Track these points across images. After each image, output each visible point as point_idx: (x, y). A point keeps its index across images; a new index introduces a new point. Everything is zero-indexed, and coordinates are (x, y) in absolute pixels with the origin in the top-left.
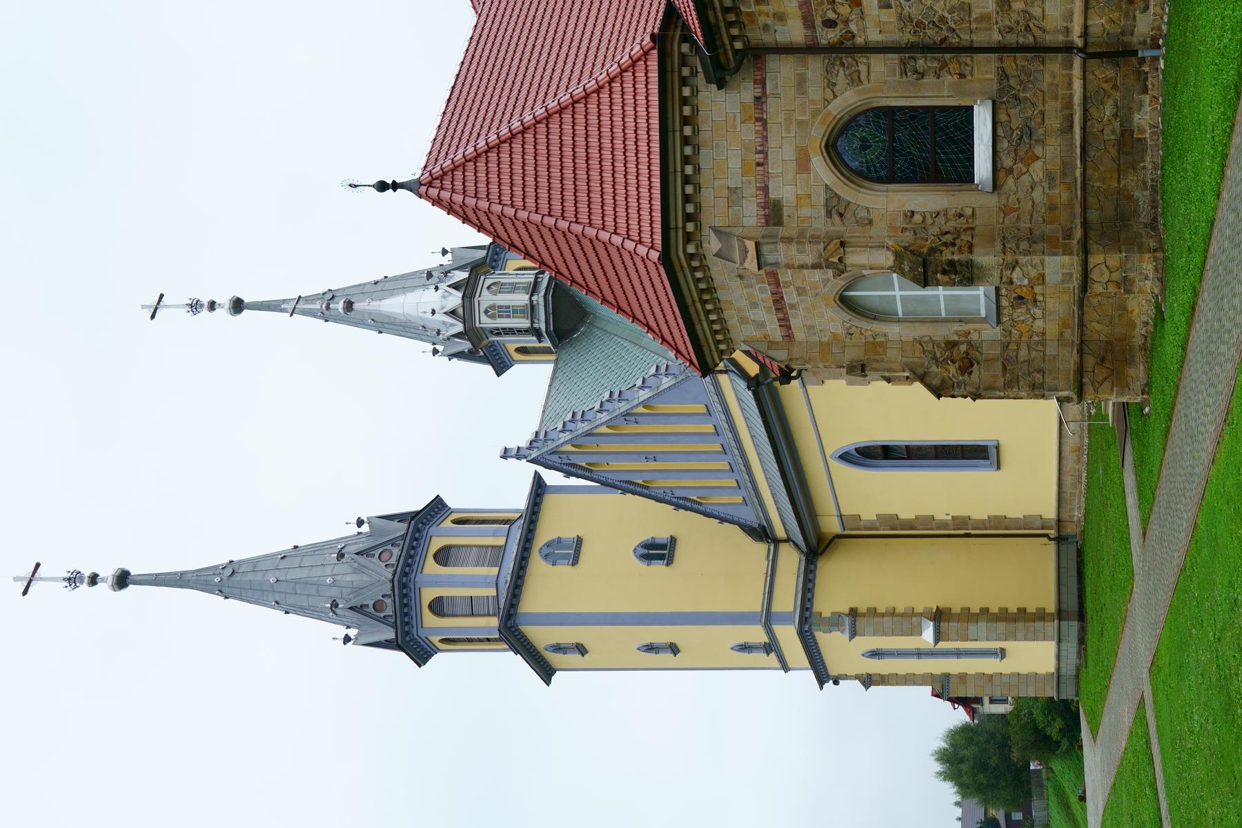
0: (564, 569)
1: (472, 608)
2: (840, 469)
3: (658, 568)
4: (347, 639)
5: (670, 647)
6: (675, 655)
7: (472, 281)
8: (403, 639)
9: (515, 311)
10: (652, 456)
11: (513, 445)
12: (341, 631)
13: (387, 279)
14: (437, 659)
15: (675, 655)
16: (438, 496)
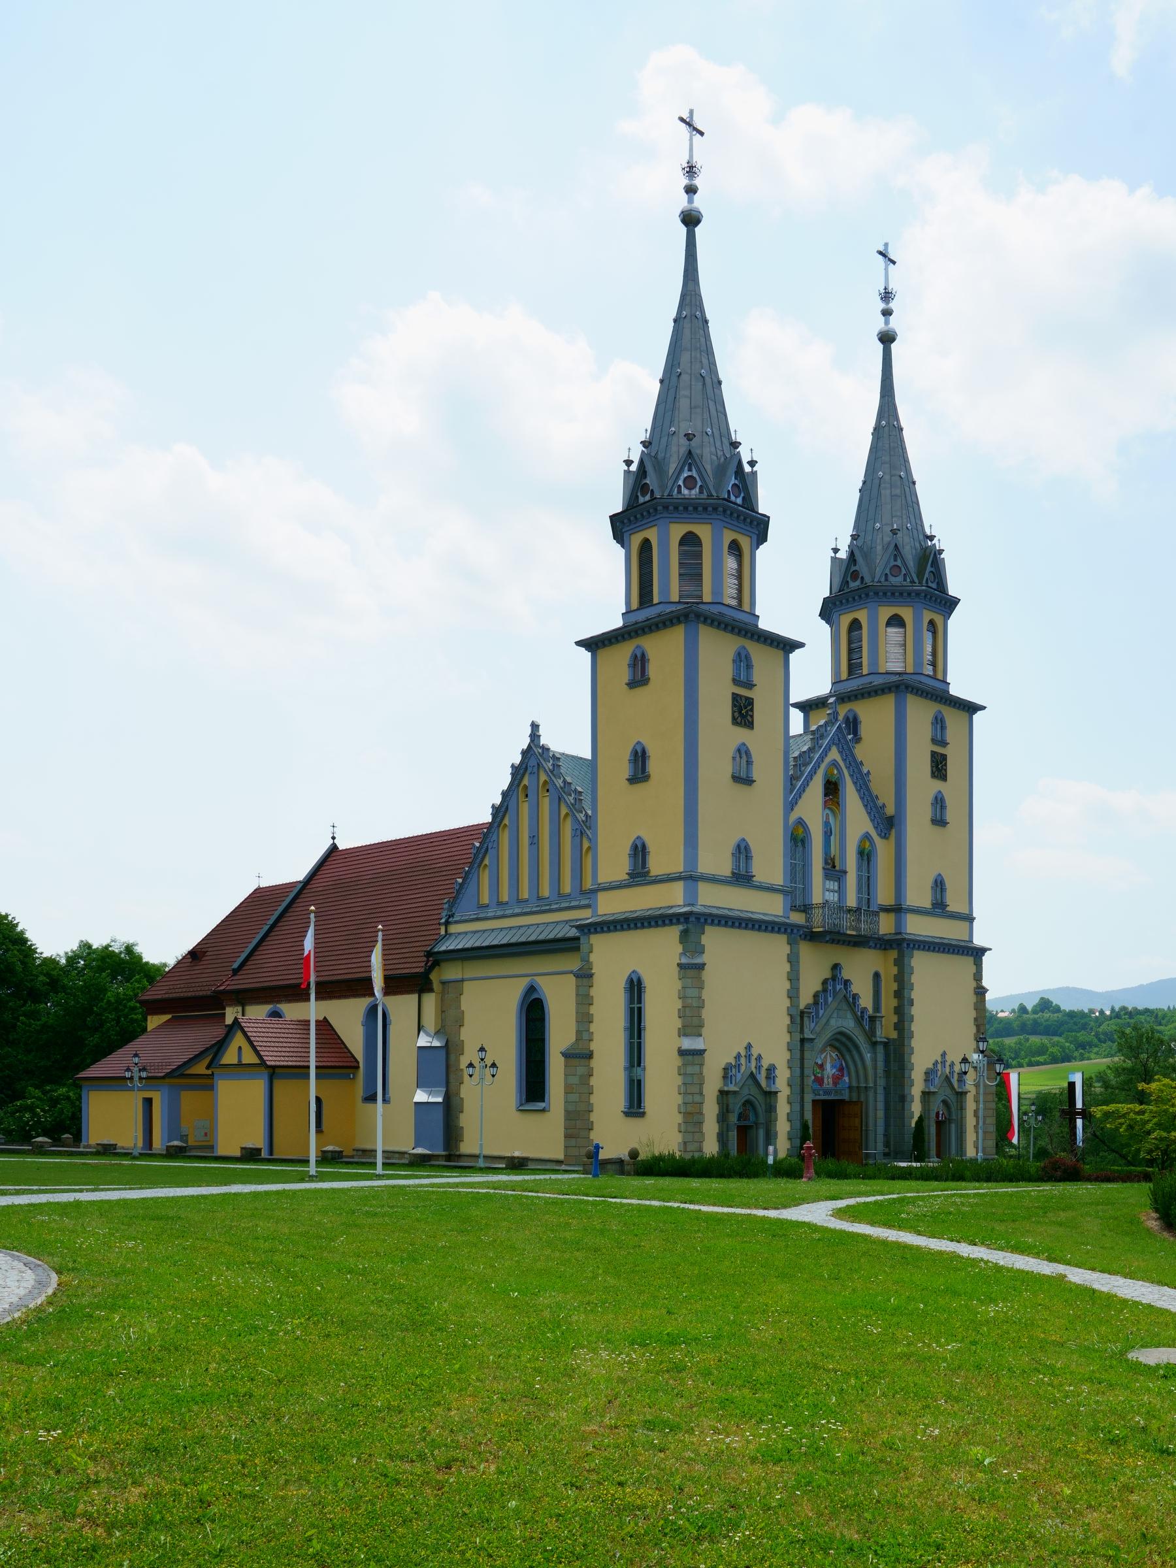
1: (691, 572)
2: (520, 986)
4: (836, 550)
10: (535, 841)
11: (541, 731)
12: (636, 458)
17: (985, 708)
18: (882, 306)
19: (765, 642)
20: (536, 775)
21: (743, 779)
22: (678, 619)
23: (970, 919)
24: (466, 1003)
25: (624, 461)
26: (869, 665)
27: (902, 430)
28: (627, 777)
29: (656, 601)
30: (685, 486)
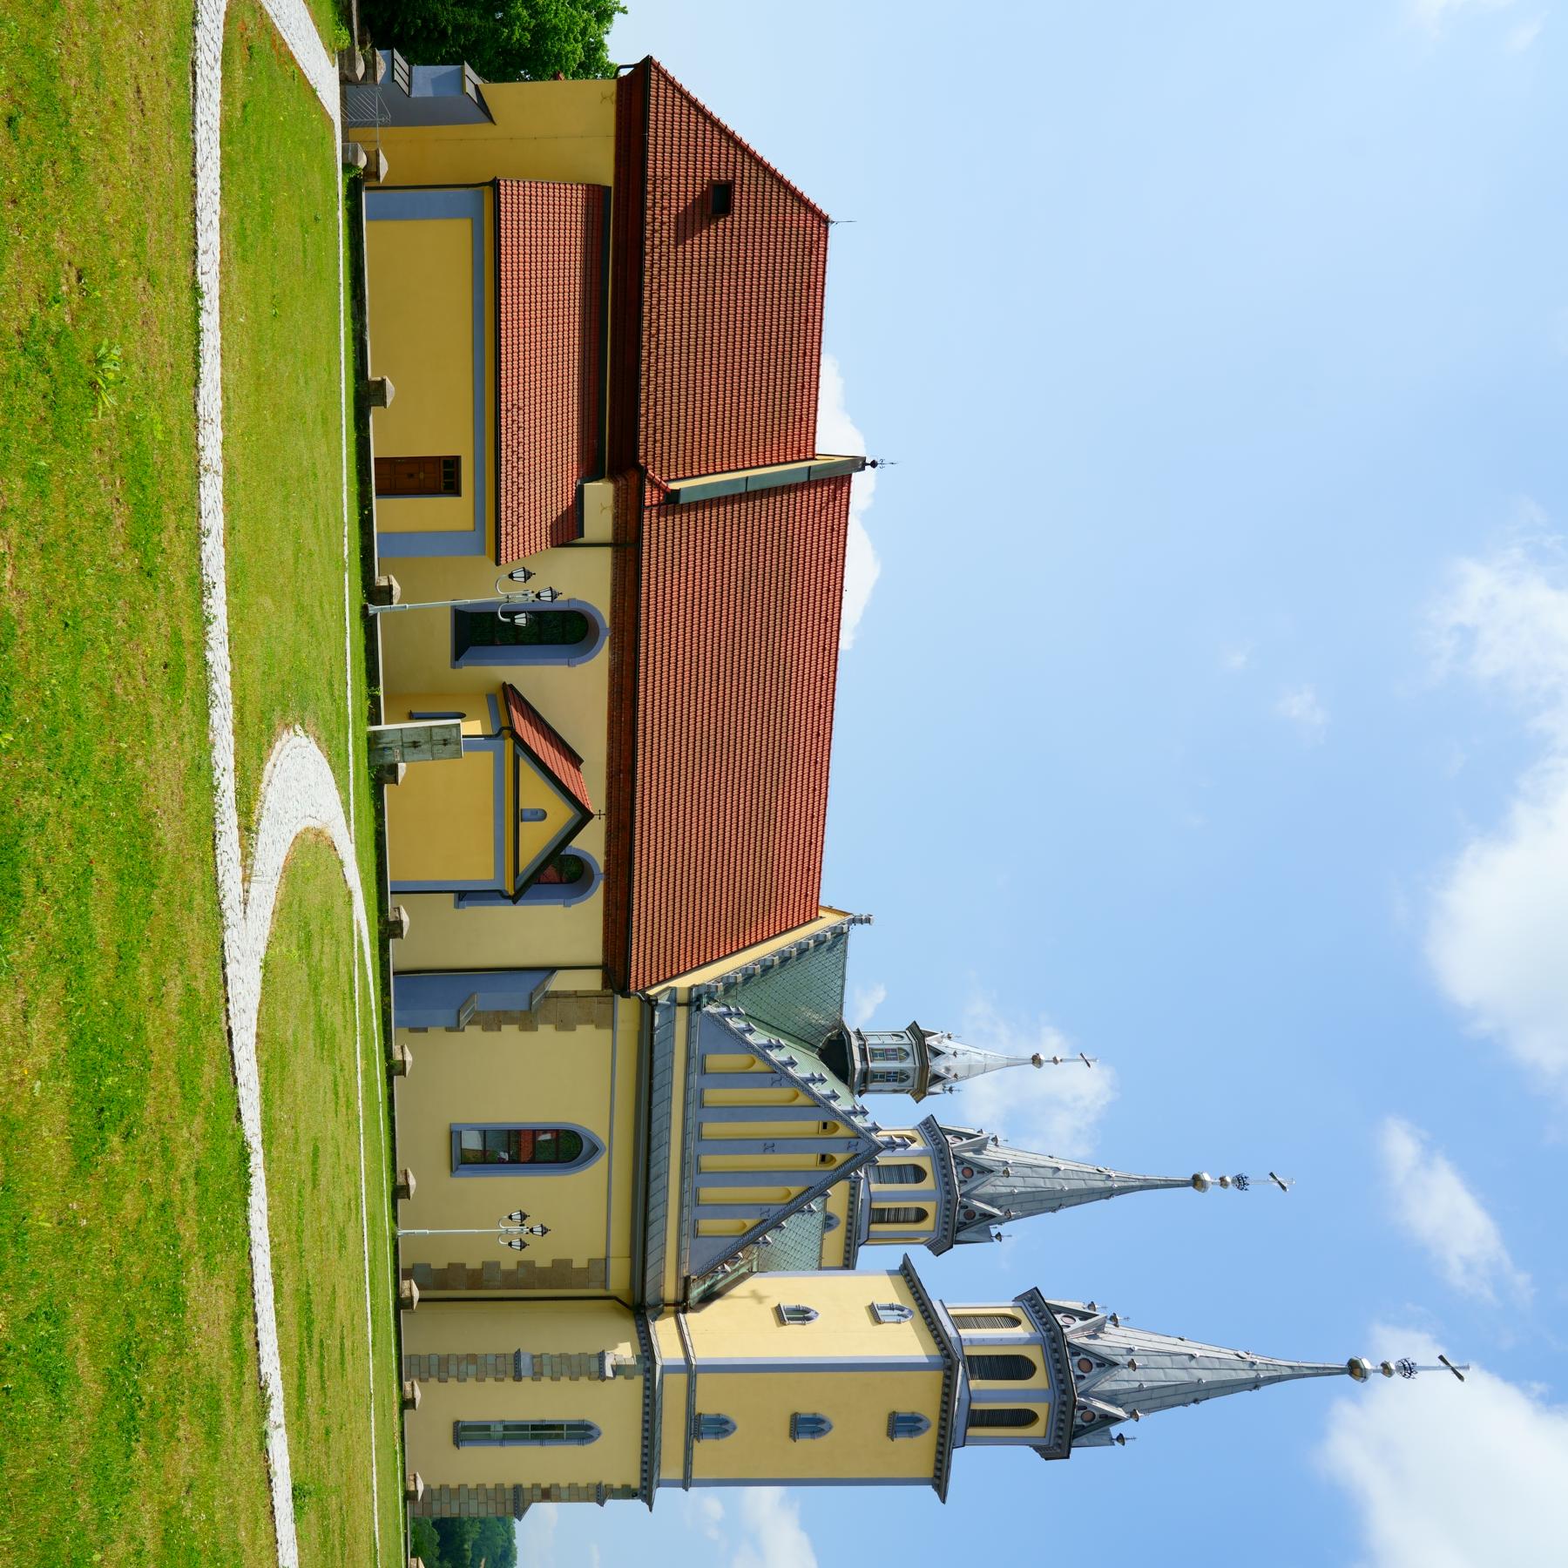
0: (904, 1408)
3: (806, 1409)
17: (944, 1502)
19: (939, 1461)
20: (775, 1142)
21: (802, 1315)
22: (945, 1349)
23: (686, 1483)
24: (585, 1031)
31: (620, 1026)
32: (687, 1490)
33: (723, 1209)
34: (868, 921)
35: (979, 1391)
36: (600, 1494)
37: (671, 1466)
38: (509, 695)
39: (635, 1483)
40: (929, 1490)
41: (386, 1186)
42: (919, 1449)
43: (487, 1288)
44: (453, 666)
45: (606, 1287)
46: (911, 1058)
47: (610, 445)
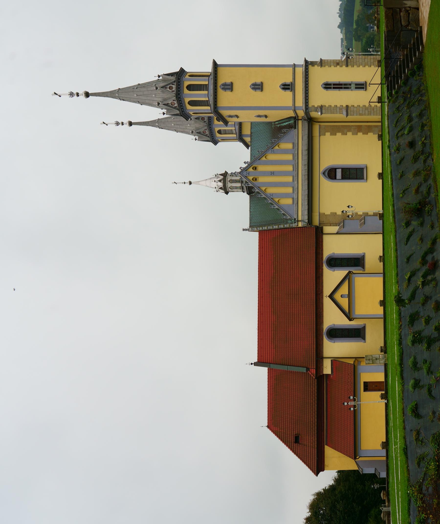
0: (228, 93)
3: (258, 93)
4: (196, 139)
5: (265, 116)
6: (266, 118)
7: (225, 179)
8: (182, 113)
9: (237, 181)
12: (194, 137)
13: (139, 85)
14: (219, 144)
15: (266, 118)
16: (181, 68)
18: (120, 125)
23: (294, 66)
24: (328, 212)
25: (164, 115)
26: (232, 127)
27: (159, 119)
28: (265, 118)
29: (207, 99)
30: (172, 89)
31: (318, 214)
32: (294, 64)
33: (286, 152)
34: (244, 230)
35: (205, 97)
36: (322, 63)
37: (300, 72)
38: (350, 320)
39: (310, 67)
40: (218, 63)
41: (383, 137)
42: (223, 79)
43: (356, 126)
44: (365, 324)
45: (320, 125)
46: (229, 187)
47: (324, 381)
